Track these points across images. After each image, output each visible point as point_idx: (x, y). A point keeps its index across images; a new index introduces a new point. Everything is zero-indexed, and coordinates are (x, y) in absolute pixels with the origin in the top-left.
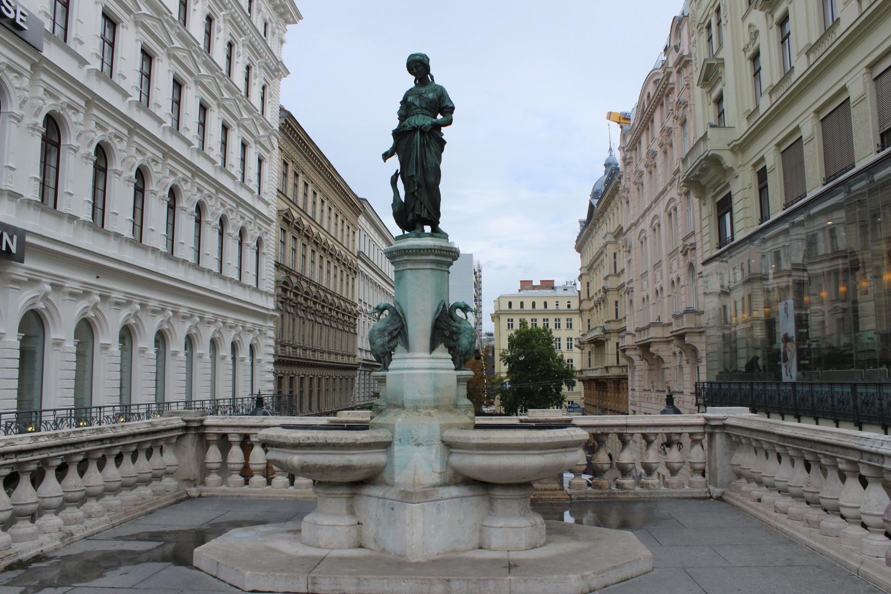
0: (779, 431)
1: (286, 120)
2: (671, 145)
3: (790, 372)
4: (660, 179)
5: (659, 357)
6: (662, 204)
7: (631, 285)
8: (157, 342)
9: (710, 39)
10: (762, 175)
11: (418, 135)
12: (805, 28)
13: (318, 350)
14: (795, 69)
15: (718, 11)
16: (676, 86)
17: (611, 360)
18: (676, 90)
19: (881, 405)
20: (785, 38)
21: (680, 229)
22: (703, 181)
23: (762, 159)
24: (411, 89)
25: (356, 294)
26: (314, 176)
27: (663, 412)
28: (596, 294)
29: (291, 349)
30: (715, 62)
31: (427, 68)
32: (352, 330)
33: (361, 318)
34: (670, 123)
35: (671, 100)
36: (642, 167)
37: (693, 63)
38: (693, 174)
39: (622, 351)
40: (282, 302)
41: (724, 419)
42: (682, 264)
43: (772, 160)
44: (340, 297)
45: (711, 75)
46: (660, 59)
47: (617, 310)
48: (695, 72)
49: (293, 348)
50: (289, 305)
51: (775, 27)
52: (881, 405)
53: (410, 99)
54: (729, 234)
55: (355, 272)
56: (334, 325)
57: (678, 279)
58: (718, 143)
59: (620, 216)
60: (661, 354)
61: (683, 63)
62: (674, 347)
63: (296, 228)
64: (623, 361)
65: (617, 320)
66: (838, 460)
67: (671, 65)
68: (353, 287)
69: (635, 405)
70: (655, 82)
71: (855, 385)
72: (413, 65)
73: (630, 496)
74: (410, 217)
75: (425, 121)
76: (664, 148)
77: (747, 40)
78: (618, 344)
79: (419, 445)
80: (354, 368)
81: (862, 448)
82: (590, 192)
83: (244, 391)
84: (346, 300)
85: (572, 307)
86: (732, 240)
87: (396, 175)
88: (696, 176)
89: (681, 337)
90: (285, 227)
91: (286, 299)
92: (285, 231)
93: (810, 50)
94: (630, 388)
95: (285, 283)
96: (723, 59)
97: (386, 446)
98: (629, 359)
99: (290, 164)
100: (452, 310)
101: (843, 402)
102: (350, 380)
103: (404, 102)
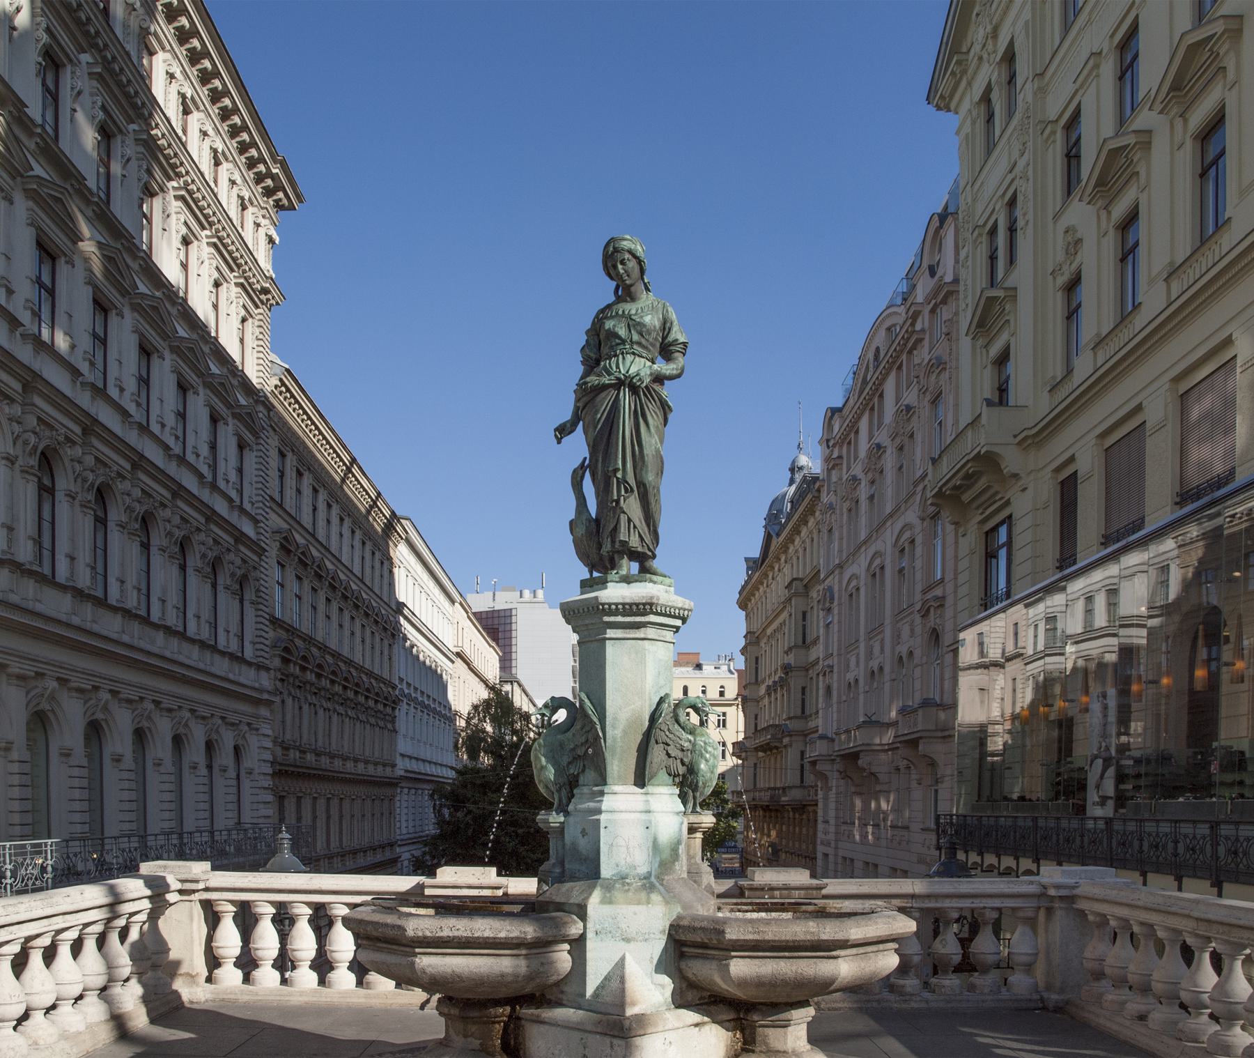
1: (281, 380)
2: (912, 436)
6: (889, 536)
7: (829, 662)
8: (87, 738)
10: (1068, 489)
13: (338, 756)
15: (1012, 203)
17: (791, 778)
18: (926, 343)
20: (1127, 254)
21: (918, 576)
28: (770, 676)
29: (297, 753)
30: (1001, 294)
32: (390, 726)
34: (911, 397)
35: (917, 361)
36: (857, 470)
37: (961, 296)
38: (950, 485)
40: (282, 680)
41: (1074, 888)
42: (918, 630)
44: (370, 674)
45: (989, 318)
46: (900, 290)
47: (803, 700)
48: (965, 311)
51: (1112, 232)
54: (1002, 584)
55: (393, 635)
57: (911, 654)
58: (995, 432)
61: (944, 295)
69: (828, 844)
70: (889, 329)
73: (914, 1005)
74: (607, 547)
75: (638, 366)
76: (898, 441)
77: (1060, 256)
78: (802, 753)
80: (393, 783)
83: (224, 819)
84: (379, 679)
86: (1008, 594)
88: (956, 488)
89: (913, 743)
93: (1173, 272)
94: (820, 819)
95: (286, 649)
98: (823, 777)
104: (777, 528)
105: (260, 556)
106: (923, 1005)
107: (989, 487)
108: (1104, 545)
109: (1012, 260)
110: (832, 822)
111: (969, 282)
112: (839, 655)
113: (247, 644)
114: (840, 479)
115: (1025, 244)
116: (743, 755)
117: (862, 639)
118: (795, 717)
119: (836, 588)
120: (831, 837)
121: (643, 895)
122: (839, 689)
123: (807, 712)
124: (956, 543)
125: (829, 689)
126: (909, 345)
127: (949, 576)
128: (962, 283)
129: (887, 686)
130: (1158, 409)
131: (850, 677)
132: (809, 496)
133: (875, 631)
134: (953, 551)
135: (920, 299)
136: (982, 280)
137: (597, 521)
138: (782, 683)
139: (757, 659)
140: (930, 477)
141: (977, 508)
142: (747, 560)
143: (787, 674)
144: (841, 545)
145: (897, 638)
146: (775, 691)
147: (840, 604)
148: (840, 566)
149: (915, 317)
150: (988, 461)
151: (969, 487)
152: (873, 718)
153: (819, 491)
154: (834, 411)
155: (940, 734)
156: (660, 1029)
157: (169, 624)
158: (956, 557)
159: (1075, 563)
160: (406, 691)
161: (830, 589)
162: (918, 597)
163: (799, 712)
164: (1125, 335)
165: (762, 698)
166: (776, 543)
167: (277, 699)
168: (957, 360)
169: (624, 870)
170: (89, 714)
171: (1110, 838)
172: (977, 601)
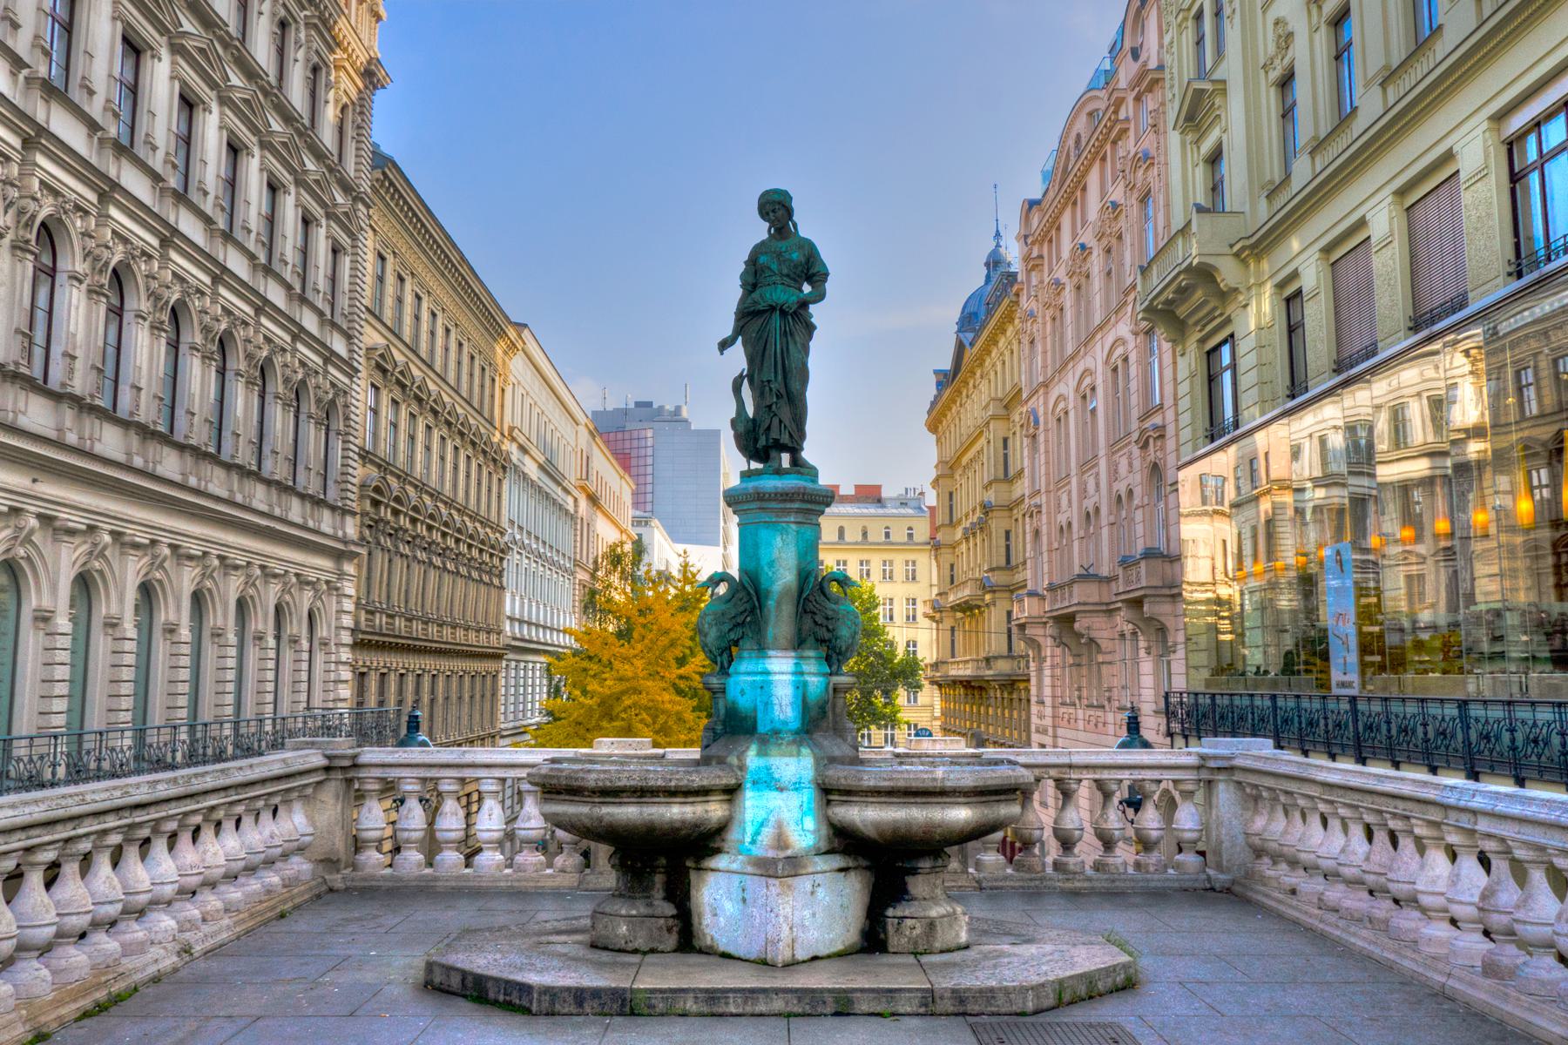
0: (1322, 776)
2: (1120, 237)
3: (1345, 671)
4: (1098, 301)
5: (1092, 640)
6: (1099, 351)
7: (1037, 500)
9: (1200, 42)
11: (776, 318)
12: (1378, 31)
14: (1360, 112)
16: (1132, 126)
17: (997, 644)
18: (1131, 133)
19: (1513, 740)
21: (1134, 399)
22: (1182, 311)
23: (1295, 275)
24: (763, 243)
25: (504, 511)
26: (431, 281)
27: (1123, 745)
30: (1208, 86)
31: (789, 212)
32: (496, 581)
33: (514, 558)
34: (1117, 194)
35: (1121, 153)
36: (1061, 273)
37: (1167, 85)
38: (1162, 298)
39: (1016, 629)
40: (370, 527)
41: (1230, 759)
42: (1137, 464)
43: (1312, 276)
45: (1198, 112)
47: (1008, 547)
49: (389, 616)
50: (383, 532)
51: (1323, 28)
52: (1513, 740)
53: (763, 259)
56: (475, 574)
57: (1130, 492)
59: (1010, 364)
60: (1094, 634)
62: (1122, 621)
63: (399, 382)
64: (1020, 646)
65: (1008, 566)
66: (1413, 821)
67: (1123, 84)
68: (499, 497)
69: (1045, 732)
70: (1090, 114)
71: (1466, 702)
72: (769, 208)
74: (762, 442)
75: (782, 295)
76: (1105, 242)
77: (1272, 49)
79: (781, 790)
81: (1446, 801)
82: (955, 314)
84: (485, 523)
85: (916, 538)
86: (1236, 425)
87: (741, 377)
88: (1168, 302)
90: (379, 381)
91: (376, 522)
92: (377, 388)
93: (1389, 77)
94: (1034, 699)
96: (1224, 82)
97: (731, 792)
98: (1033, 643)
99: (390, 258)
100: (825, 584)
101: (1443, 733)
102: (489, 678)
103: (753, 262)
104: (970, 336)
105: (351, 377)
106: (1086, 884)
107: (1205, 303)
108: (1337, 371)
109: (1219, 52)
110: (1048, 701)
111: (1175, 70)
112: (1048, 492)
113: (330, 483)
114: (1042, 282)
115: (1233, 34)
116: (938, 616)
117: (1073, 472)
118: (999, 568)
119: (1041, 411)
120: (1048, 722)
121: (794, 749)
122: (1049, 534)
123: (1013, 563)
124: (1175, 363)
125: (1037, 533)
126: (1113, 135)
127: (1169, 402)
128: (1167, 70)
129: (1105, 532)
130: (1312, 276)
131: (1062, 519)
132: (1006, 301)
133: (1088, 464)
134: (1174, 370)
135: (1123, 84)
136: (1189, 71)
137: (754, 420)
138: (981, 526)
139: (951, 494)
140: (1139, 288)
141: (1196, 324)
142: (936, 372)
143: (986, 514)
144: (1044, 360)
145: (1114, 474)
146: (974, 534)
147: (1046, 430)
148: (1046, 385)
149: (1119, 103)
150: (1204, 274)
151: (1185, 300)
152: (1091, 571)
153: (1017, 295)
154: (1032, 204)
155: (1167, 592)
156: (810, 870)
157: (78, 391)
158: (1175, 379)
159: (1307, 390)
160: (518, 537)
161: (1034, 412)
162: (1135, 425)
163: (1003, 562)
164: (1420, 68)
165: (959, 543)
166: (970, 353)
167: (363, 551)
168: (1166, 155)
169: (778, 726)
170: (143, 572)
171: (1356, 721)
172: (1201, 433)
